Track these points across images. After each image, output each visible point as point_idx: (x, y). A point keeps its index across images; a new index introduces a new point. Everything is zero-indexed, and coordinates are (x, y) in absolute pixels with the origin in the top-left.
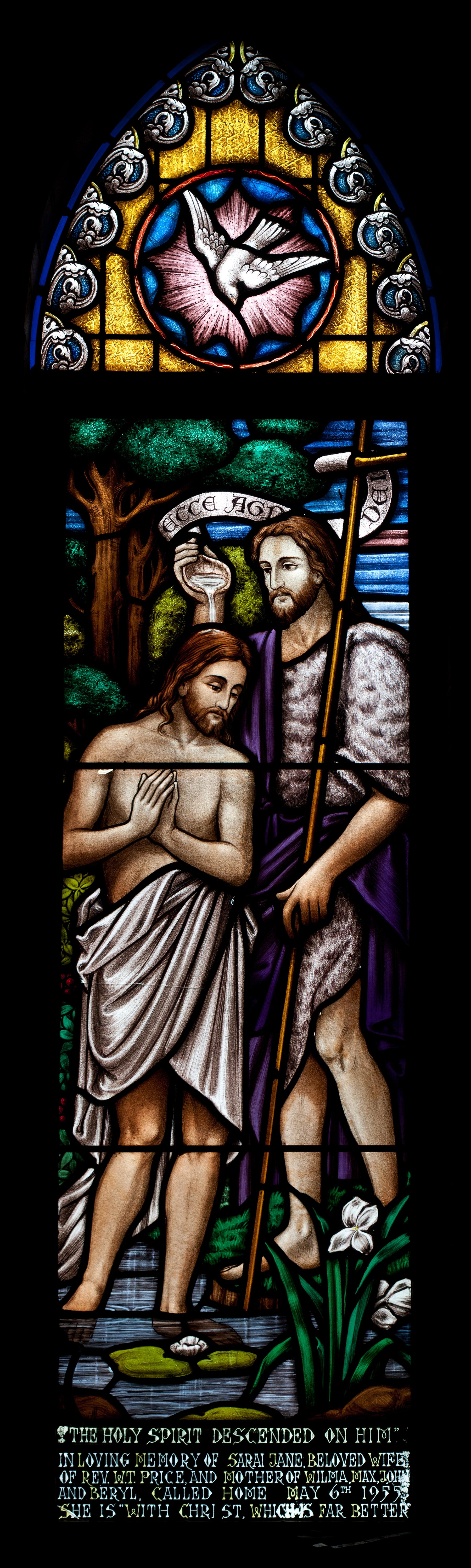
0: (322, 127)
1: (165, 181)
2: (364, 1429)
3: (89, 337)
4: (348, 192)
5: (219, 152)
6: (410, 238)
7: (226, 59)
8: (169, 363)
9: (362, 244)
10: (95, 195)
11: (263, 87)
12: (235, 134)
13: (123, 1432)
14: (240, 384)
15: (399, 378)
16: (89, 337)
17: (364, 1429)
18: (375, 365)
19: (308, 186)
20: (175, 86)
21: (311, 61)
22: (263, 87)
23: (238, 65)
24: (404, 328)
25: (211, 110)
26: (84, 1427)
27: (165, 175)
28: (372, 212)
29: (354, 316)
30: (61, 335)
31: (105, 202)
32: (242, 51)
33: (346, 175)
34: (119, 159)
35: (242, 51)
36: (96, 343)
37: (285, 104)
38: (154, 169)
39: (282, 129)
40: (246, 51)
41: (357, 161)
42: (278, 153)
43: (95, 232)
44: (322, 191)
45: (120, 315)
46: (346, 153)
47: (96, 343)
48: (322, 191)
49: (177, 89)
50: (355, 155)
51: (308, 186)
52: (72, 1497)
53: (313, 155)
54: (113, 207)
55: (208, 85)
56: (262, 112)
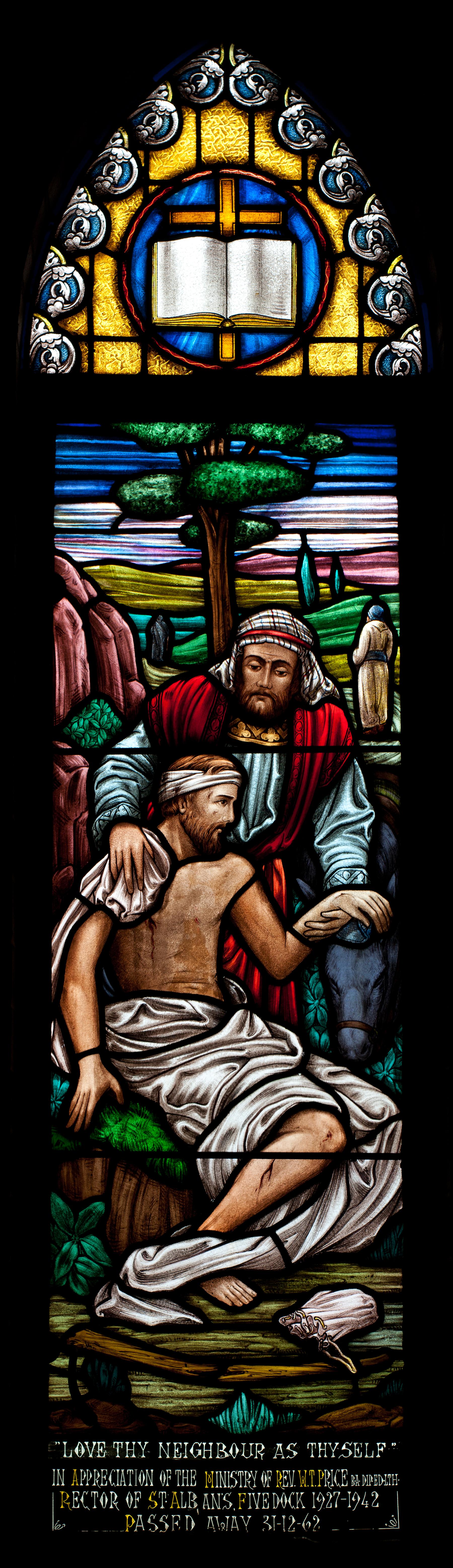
0: (400, 304)
1: (154, 182)
2: (211, 1444)
3: (75, 338)
4: (364, 248)
5: (209, 153)
6: (400, 239)
7: (217, 61)
8: (159, 367)
9: (353, 245)
10: (84, 196)
11: (254, 88)
12: (224, 134)
13: (85, 1445)
14: (226, 382)
15: (390, 380)
16: (75, 338)
17: (211, 1444)
18: (366, 368)
19: (297, 188)
20: (164, 87)
21: (301, 67)
22: (254, 88)
23: (228, 68)
24: (396, 331)
25: (200, 110)
26: (96, 1441)
27: (154, 175)
28: (363, 215)
29: (343, 316)
30: (50, 337)
31: (93, 203)
32: (231, 53)
33: (336, 174)
34: (107, 160)
35: (231, 53)
36: (84, 348)
37: (275, 107)
38: (144, 171)
39: (273, 131)
40: (236, 53)
41: (348, 161)
42: (268, 155)
43: (84, 233)
44: (312, 196)
45: (109, 318)
46: (394, 270)
47: (84, 348)
48: (312, 196)
49: (167, 90)
50: (403, 276)
51: (297, 188)
52: (216, 1496)
53: (303, 155)
54: (102, 208)
55: (196, 85)
56: (250, 114)
